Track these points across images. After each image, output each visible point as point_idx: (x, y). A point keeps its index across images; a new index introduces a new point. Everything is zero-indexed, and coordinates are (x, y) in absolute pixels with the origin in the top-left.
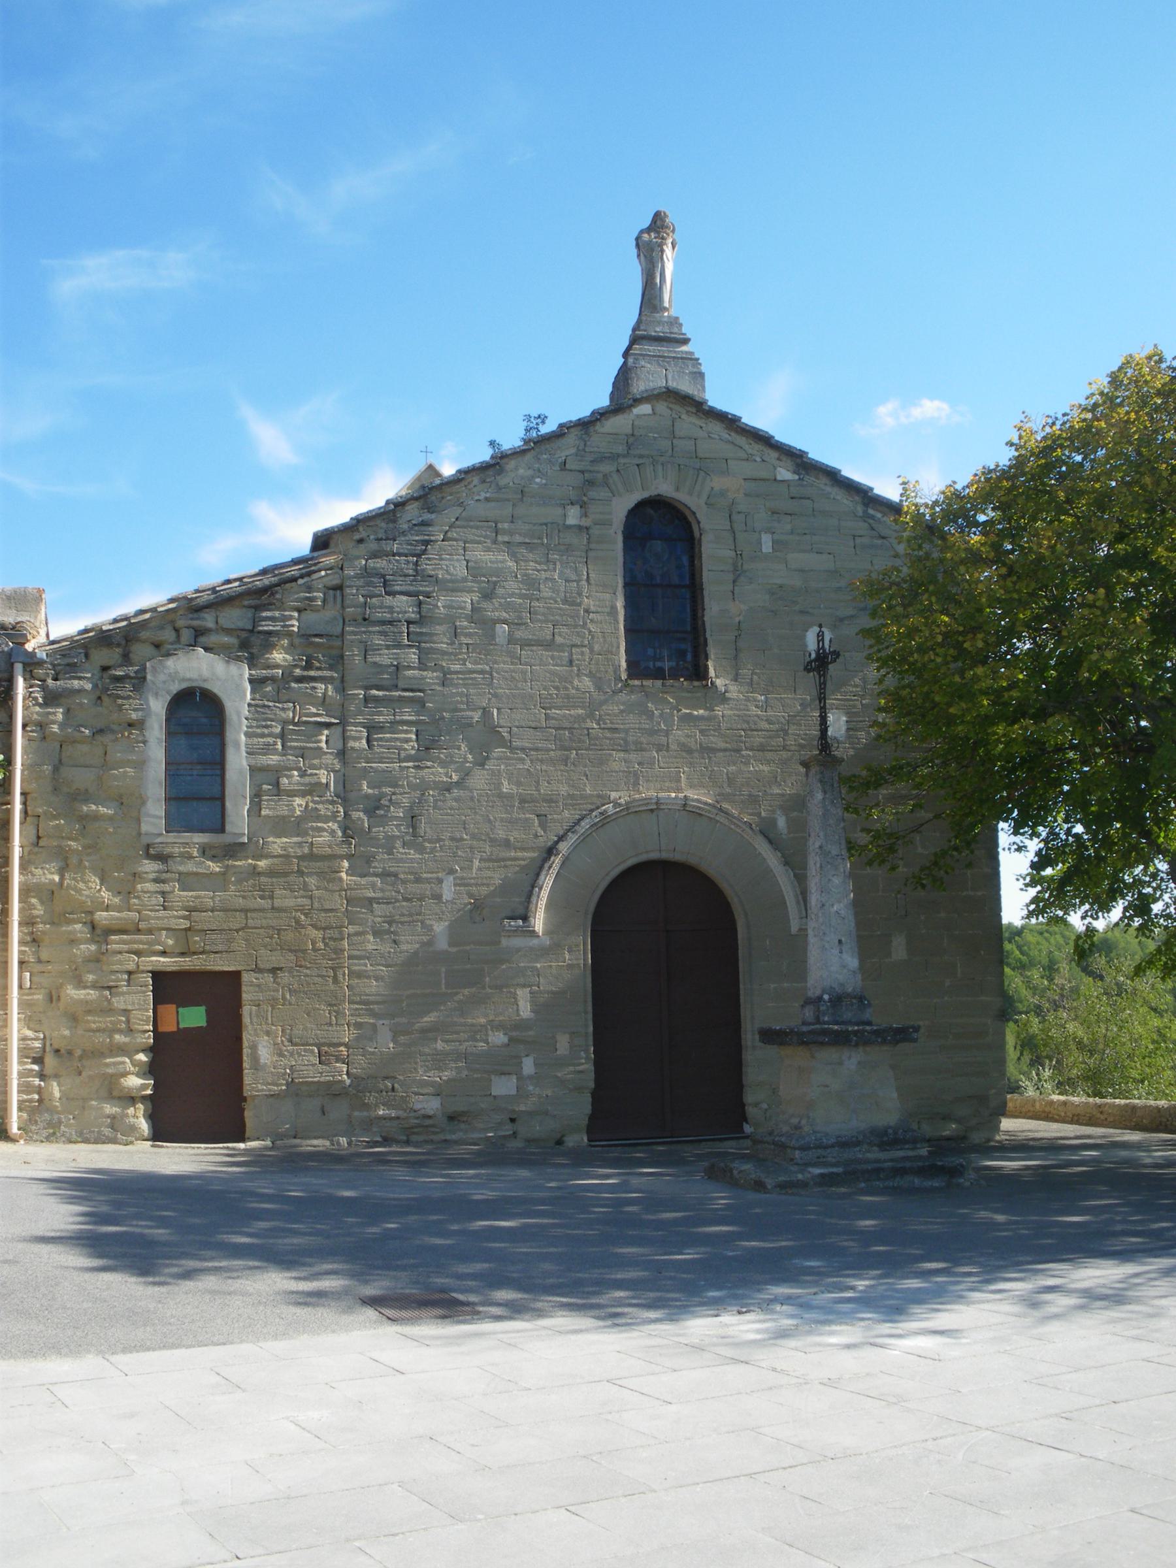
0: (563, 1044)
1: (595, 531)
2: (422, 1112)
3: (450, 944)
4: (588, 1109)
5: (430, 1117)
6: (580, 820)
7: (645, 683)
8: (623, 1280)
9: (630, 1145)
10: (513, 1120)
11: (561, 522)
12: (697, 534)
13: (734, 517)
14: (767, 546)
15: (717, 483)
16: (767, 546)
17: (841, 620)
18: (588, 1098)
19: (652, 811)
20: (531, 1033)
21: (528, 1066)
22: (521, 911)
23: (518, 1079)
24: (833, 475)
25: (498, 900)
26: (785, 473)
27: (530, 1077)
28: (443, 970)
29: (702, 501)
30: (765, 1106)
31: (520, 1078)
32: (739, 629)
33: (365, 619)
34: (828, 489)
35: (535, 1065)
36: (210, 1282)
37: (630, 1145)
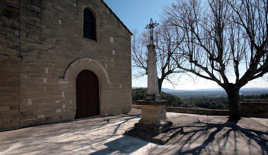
0: (71, 102)
1: (79, 9)
2: (40, 118)
3: (47, 82)
4: (75, 114)
5: (41, 119)
6: (258, 5)
7: (87, 39)
8: (20, 153)
9: (88, 118)
10: (60, 117)
11: (73, 5)
12: (95, 17)
13: (101, 16)
14: (106, 23)
15: (99, 10)
16: (106, 23)
17: (115, 37)
18: (75, 112)
19: (87, 61)
20: (65, 100)
21: (64, 106)
22: (63, 76)
23: (62, 110)
24: (115, 15)
25: (58, 74)
26: (108, 12)
27: (64, 109)
28: (45, 88)
29: (97, 11)
30: (103, 110)
31: (62, 109)
32: (101, 34)
33: (26, 7)
34: (114, 17)
35: (65, 106)
36: (136, 151)
37: (89, 118)
